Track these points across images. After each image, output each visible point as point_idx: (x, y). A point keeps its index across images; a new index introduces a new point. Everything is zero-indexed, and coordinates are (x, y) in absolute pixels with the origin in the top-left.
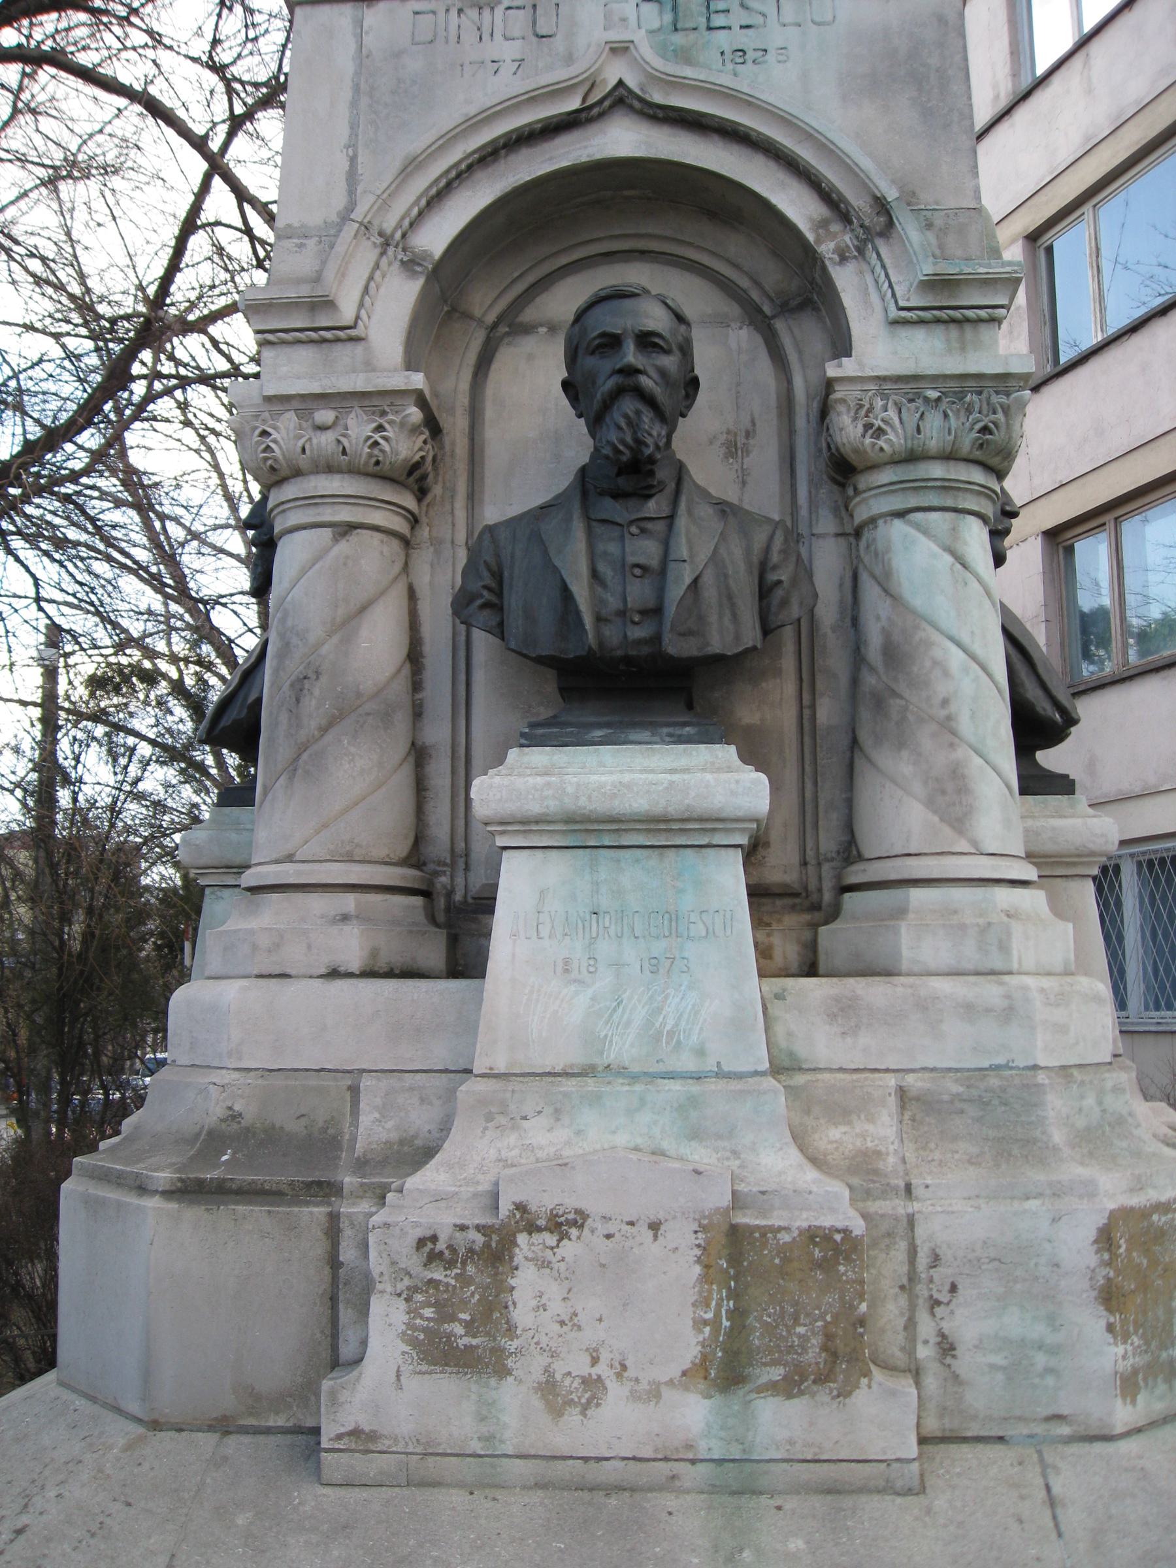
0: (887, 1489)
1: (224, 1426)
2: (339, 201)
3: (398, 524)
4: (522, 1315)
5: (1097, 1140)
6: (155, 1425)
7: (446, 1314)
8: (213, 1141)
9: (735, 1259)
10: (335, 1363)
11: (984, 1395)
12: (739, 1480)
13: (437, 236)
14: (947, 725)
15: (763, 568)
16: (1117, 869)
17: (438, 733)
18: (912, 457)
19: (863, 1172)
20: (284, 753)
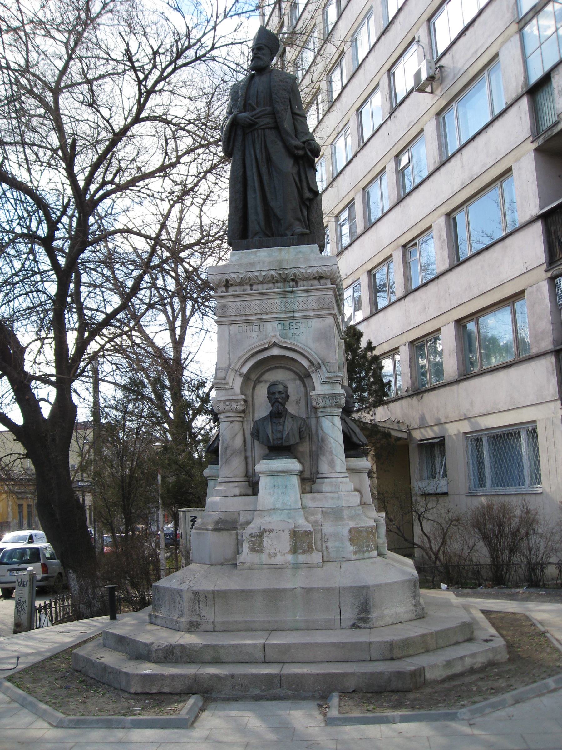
0: (318, 567)
1: (222, 564)
2: (228, 363)
3: (241, 419)
4: (265, 544)
5: (352, 518)
6: (212, 565)
7: (254, 544)
8: (217, 523)
9: (295, 535)
10: (238, 554)
11: (333, 555)
12: (296, 567)
13: (245, 370)
14: (331, 453)
15: (300, 428)
16: (481, 439)
17: (249, 454)
18: (325, 407)
19: (315, 523)
20: (224, 460)
